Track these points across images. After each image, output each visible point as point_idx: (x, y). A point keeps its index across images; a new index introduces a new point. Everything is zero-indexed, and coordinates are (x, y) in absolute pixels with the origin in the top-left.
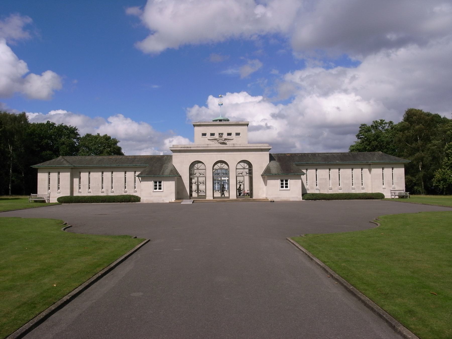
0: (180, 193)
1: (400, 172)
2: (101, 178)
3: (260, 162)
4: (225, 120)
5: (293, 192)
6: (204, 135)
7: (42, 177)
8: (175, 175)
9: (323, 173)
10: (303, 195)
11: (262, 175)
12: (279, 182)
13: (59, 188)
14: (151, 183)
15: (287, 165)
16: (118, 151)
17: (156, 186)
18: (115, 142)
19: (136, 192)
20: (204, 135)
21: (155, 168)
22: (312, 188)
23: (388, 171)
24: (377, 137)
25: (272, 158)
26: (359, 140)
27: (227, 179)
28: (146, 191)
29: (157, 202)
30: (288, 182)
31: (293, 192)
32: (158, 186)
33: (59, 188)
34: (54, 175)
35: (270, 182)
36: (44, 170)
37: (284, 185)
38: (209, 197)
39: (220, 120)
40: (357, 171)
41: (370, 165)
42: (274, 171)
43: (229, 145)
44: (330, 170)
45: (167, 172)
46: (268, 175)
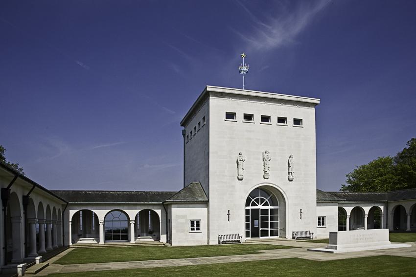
6: (230, 116)
20: (230, 116)
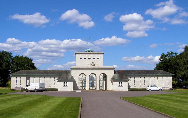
0: (75, 87)
1: (170, 79)
2: (16, 80)
3: (110, 74)
4: (91, 51)
5: (124, 87)
6: (81, 58)
7: (13, 79)
8: (73, 80)
9: (137, 79)
10: (128, 89)
11: (111, 80)
12: (118, 83)
13: (21, 85)
14: (63, 83)
15: (122, 76)
16: (33, 67)
17: (65, 84)
18: (31, 60)
19: (55, 86)
20: (81, 58)
21: (63, 76)
22: (133, 86)
23: (165, 78)
24: (169, 60)
25: (115, 72)
26: (160, 62)
27: (90, 81)
28: (61, 87)
29: (65, 91)
30: (122, 83)
31: (124, 87)
32: (65, 84)
33: (21, 85)
34: (19, 78)
35: (114, 83)
36: (14, 76)
37: (120, 84)
38: (87, 89)
39: (89, 51)
40: (152, 78)
41: (157, 77)
42: (116, 78)
43: (97, 67)
44: (140, 78)
45: (70, 78)
46: (113, 80)
